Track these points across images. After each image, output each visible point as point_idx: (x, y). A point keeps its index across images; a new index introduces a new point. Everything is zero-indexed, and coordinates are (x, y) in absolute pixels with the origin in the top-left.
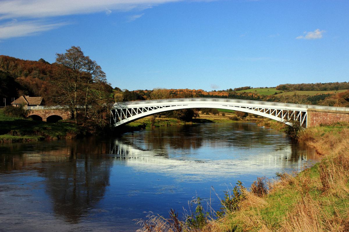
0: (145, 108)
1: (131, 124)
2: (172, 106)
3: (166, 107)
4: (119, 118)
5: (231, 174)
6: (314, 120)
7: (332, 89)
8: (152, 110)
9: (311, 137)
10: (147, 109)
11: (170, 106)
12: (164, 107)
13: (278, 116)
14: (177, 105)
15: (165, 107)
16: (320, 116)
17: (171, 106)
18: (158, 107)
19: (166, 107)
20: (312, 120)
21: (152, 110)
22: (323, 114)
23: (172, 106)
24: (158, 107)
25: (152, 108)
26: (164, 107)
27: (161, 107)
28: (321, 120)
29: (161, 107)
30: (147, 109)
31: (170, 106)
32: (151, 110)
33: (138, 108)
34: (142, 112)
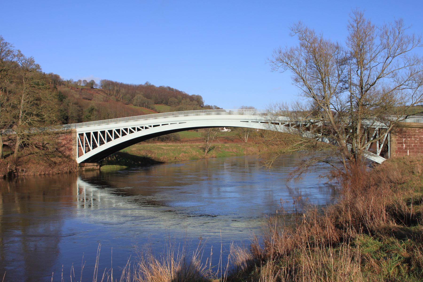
0: (124, 129)
1: (132, 150)
2: (162, 125)
3: (154, 126)
4: (245, 137)
5: (217, 234)
6: (402, 143)
7: (148, 219)
8: (133, 132)
9: (399, 199)
10: (127, 132)
11: (159, 125)
12: (151, 126)
13: (115, 139)
14: (169, 123)
15: (152, 126)
16: (415, 135)
17: (161, 125)
18: (142, 127)
19: (154, 126)
20: (398, 143)
21: (133, 132)
22: (419, 132)
23: (162, 125)
24: (142, 127)
25: (134, 129)
26: (151, 126)
27: (146, 128)
28: (417, 143)
29: (146, 128)
30: (127, 132)
31: (159, 125)
32: (140, 130)
33: (114, 130)
34: (128, 134)
